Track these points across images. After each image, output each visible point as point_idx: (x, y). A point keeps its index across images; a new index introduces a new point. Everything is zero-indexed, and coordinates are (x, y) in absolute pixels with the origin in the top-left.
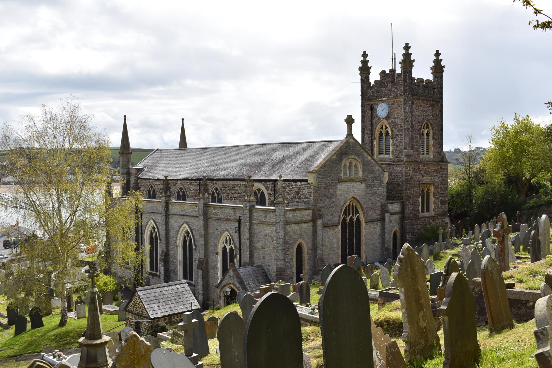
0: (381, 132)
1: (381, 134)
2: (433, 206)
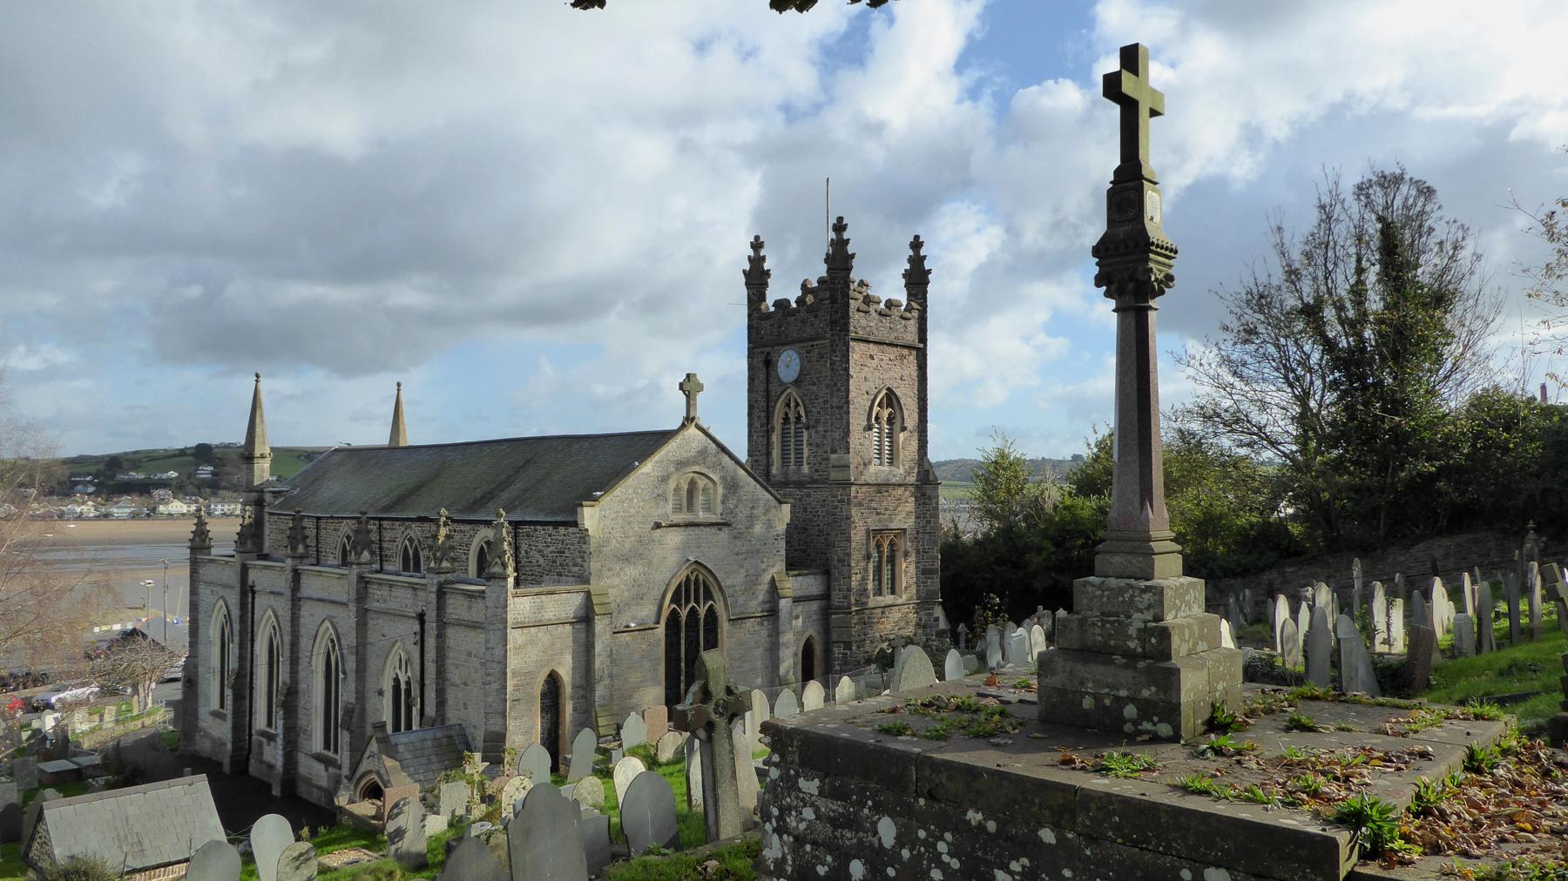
1: (786, 419)
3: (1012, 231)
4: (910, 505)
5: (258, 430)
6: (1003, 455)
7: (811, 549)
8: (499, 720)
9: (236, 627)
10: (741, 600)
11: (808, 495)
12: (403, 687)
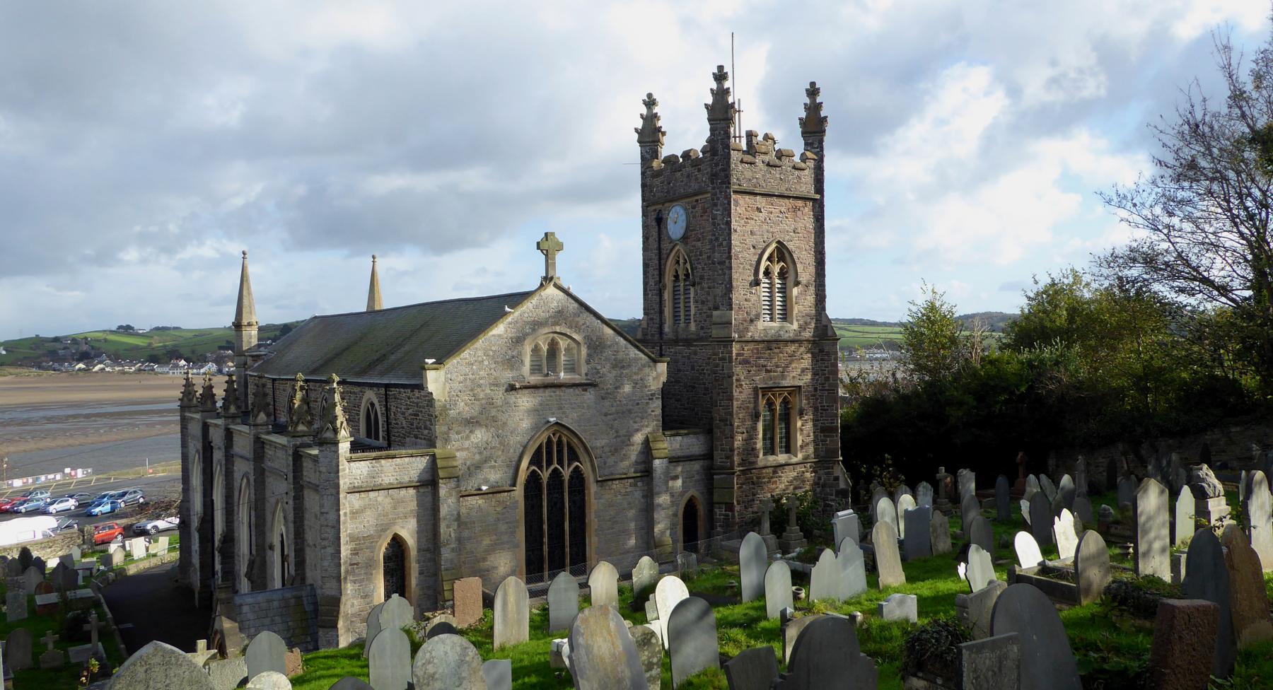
1: (677, 277)
3: (1014, 92)
4: (807, 362)
5: (245, 301)
6: (932, 308)
7: (692, 406)
8: (334, 583)
10: (611, 461)
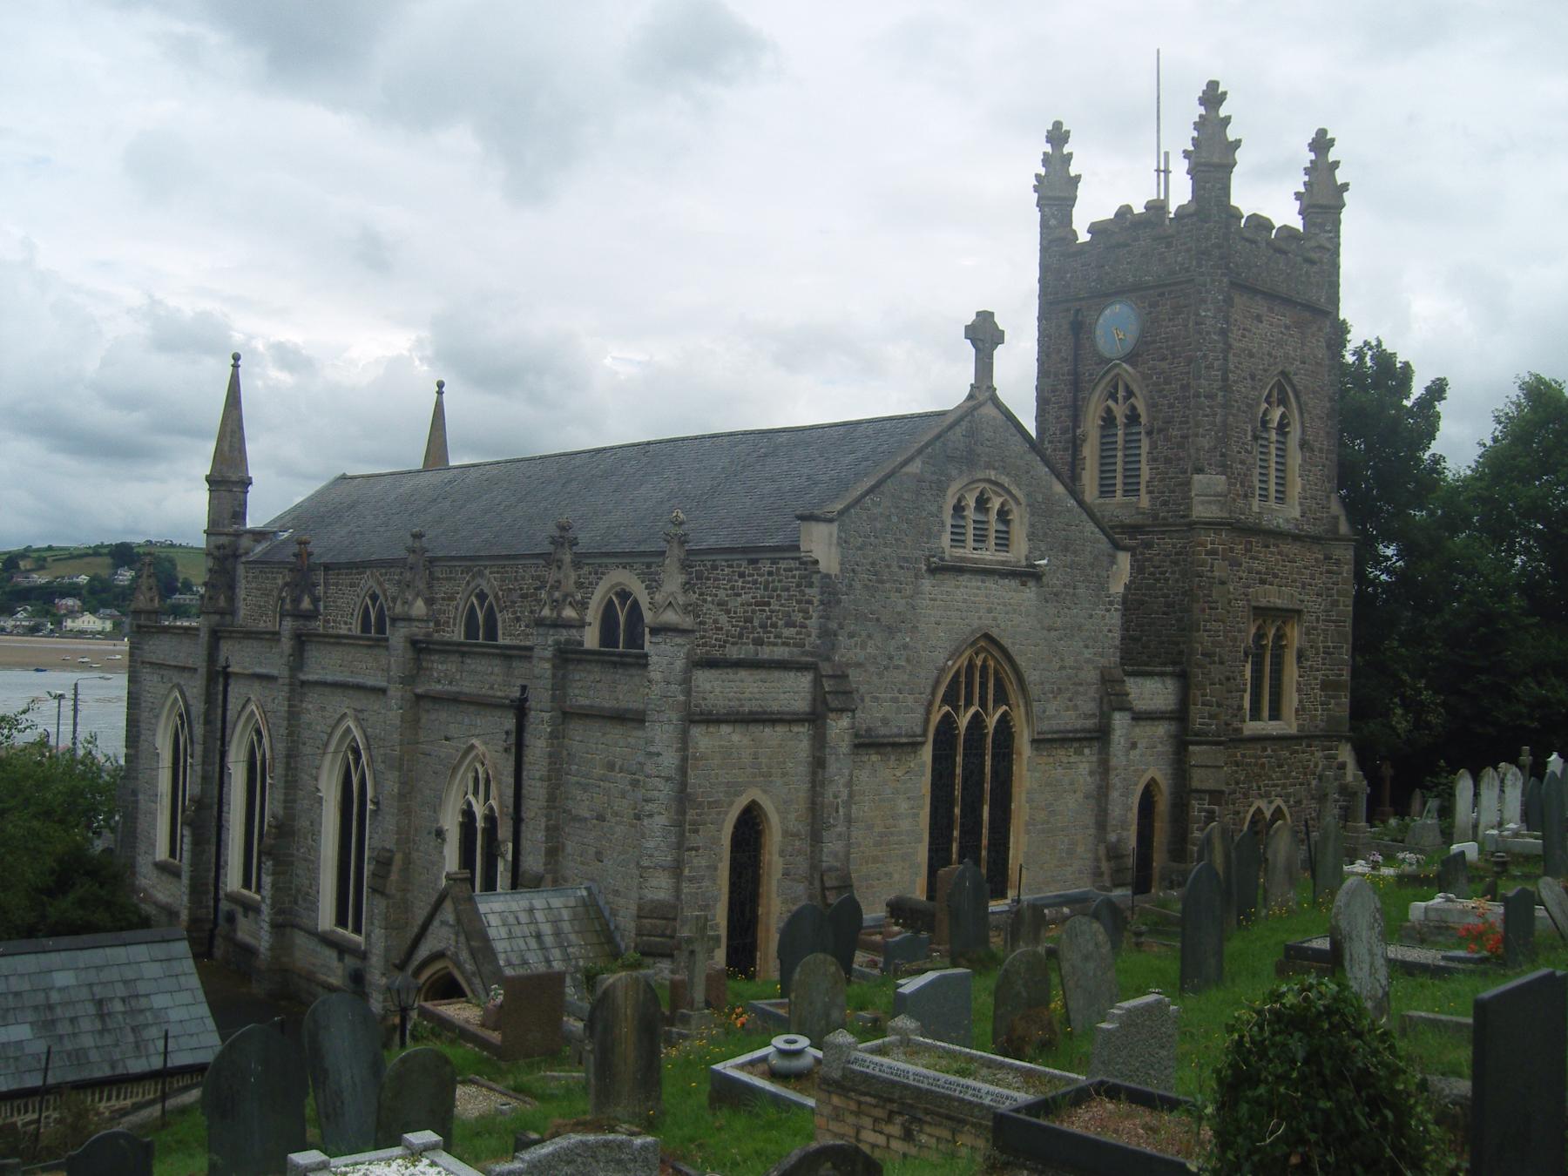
0: (1109, 410)
1: (1109, 420)
2: (1296, 697)
9: (199, 730)
11: (1149, 546)
12: (480, 824)
